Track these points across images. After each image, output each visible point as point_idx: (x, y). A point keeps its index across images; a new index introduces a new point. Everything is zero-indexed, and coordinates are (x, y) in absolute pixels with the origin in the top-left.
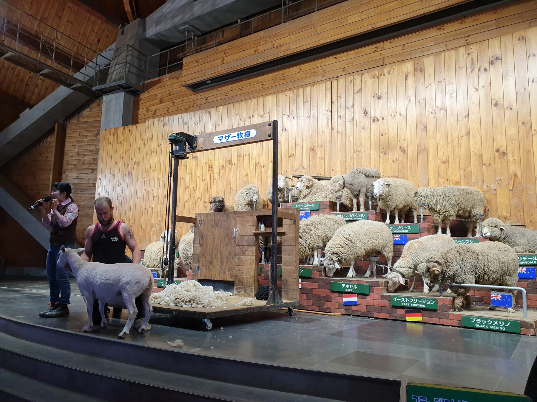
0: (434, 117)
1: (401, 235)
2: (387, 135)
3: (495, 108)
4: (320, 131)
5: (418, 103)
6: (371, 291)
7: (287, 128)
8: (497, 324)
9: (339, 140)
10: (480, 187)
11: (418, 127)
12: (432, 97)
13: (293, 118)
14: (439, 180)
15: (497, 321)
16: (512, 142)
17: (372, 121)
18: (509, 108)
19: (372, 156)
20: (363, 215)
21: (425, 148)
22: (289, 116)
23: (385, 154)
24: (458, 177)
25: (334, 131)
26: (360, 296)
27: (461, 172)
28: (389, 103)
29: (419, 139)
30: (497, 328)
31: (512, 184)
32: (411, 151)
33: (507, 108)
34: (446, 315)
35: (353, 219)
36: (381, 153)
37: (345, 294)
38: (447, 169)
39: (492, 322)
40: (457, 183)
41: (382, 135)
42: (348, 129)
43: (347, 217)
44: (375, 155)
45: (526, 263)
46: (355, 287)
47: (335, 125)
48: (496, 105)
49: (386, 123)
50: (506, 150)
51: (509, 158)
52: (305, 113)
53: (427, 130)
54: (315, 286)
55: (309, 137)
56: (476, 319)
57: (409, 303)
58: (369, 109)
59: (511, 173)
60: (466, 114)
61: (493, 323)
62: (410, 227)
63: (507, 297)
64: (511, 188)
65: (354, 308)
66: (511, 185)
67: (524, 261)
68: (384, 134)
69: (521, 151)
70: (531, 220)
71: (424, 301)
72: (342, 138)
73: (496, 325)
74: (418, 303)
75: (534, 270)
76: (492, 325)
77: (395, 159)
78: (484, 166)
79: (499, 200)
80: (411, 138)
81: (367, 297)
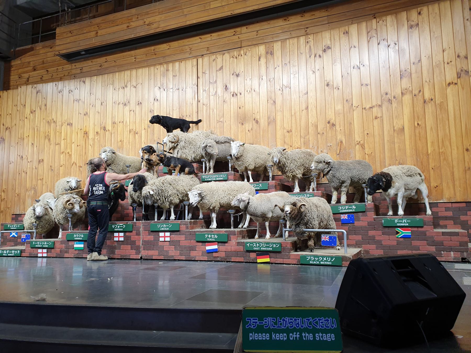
2: (244, 108)
3: (327, 88)
6: (230, 239)
7: (159, 99)
9: (204, 111)
13: (163, 90)
17: (231, 96)
18: (337, 88)
22: (160, 88)
23: (242, 124)
26: (220, 244)
27: (302, 140)
28: (245, 80)
29: (269, 112)
31: (339, 150)
32: (263, 122)
35: (216, 179)
36: (239, 124)
38: (291, 137)
39: (322, 258)
41: (240, 108)
42: (212, 102)
43: (211, 178)
45: (347, 211)
46: (216, 237)
47: (201, 98)
48: (328, 85)
49: (243, 98)
51: (337, 128)
52: (174, 86)
54: (182, 238)
55: (178, 108)
56: (310, 257)
58: (229, 85)
61: (323, 259)
65: (215, 255)
68: (241, 107)
69: (345, 123)
71: (271, 245)
72: (207, 110)
74: (266, 247)
76: (322, 261)
80: (263, 111)
81: (226, 244)
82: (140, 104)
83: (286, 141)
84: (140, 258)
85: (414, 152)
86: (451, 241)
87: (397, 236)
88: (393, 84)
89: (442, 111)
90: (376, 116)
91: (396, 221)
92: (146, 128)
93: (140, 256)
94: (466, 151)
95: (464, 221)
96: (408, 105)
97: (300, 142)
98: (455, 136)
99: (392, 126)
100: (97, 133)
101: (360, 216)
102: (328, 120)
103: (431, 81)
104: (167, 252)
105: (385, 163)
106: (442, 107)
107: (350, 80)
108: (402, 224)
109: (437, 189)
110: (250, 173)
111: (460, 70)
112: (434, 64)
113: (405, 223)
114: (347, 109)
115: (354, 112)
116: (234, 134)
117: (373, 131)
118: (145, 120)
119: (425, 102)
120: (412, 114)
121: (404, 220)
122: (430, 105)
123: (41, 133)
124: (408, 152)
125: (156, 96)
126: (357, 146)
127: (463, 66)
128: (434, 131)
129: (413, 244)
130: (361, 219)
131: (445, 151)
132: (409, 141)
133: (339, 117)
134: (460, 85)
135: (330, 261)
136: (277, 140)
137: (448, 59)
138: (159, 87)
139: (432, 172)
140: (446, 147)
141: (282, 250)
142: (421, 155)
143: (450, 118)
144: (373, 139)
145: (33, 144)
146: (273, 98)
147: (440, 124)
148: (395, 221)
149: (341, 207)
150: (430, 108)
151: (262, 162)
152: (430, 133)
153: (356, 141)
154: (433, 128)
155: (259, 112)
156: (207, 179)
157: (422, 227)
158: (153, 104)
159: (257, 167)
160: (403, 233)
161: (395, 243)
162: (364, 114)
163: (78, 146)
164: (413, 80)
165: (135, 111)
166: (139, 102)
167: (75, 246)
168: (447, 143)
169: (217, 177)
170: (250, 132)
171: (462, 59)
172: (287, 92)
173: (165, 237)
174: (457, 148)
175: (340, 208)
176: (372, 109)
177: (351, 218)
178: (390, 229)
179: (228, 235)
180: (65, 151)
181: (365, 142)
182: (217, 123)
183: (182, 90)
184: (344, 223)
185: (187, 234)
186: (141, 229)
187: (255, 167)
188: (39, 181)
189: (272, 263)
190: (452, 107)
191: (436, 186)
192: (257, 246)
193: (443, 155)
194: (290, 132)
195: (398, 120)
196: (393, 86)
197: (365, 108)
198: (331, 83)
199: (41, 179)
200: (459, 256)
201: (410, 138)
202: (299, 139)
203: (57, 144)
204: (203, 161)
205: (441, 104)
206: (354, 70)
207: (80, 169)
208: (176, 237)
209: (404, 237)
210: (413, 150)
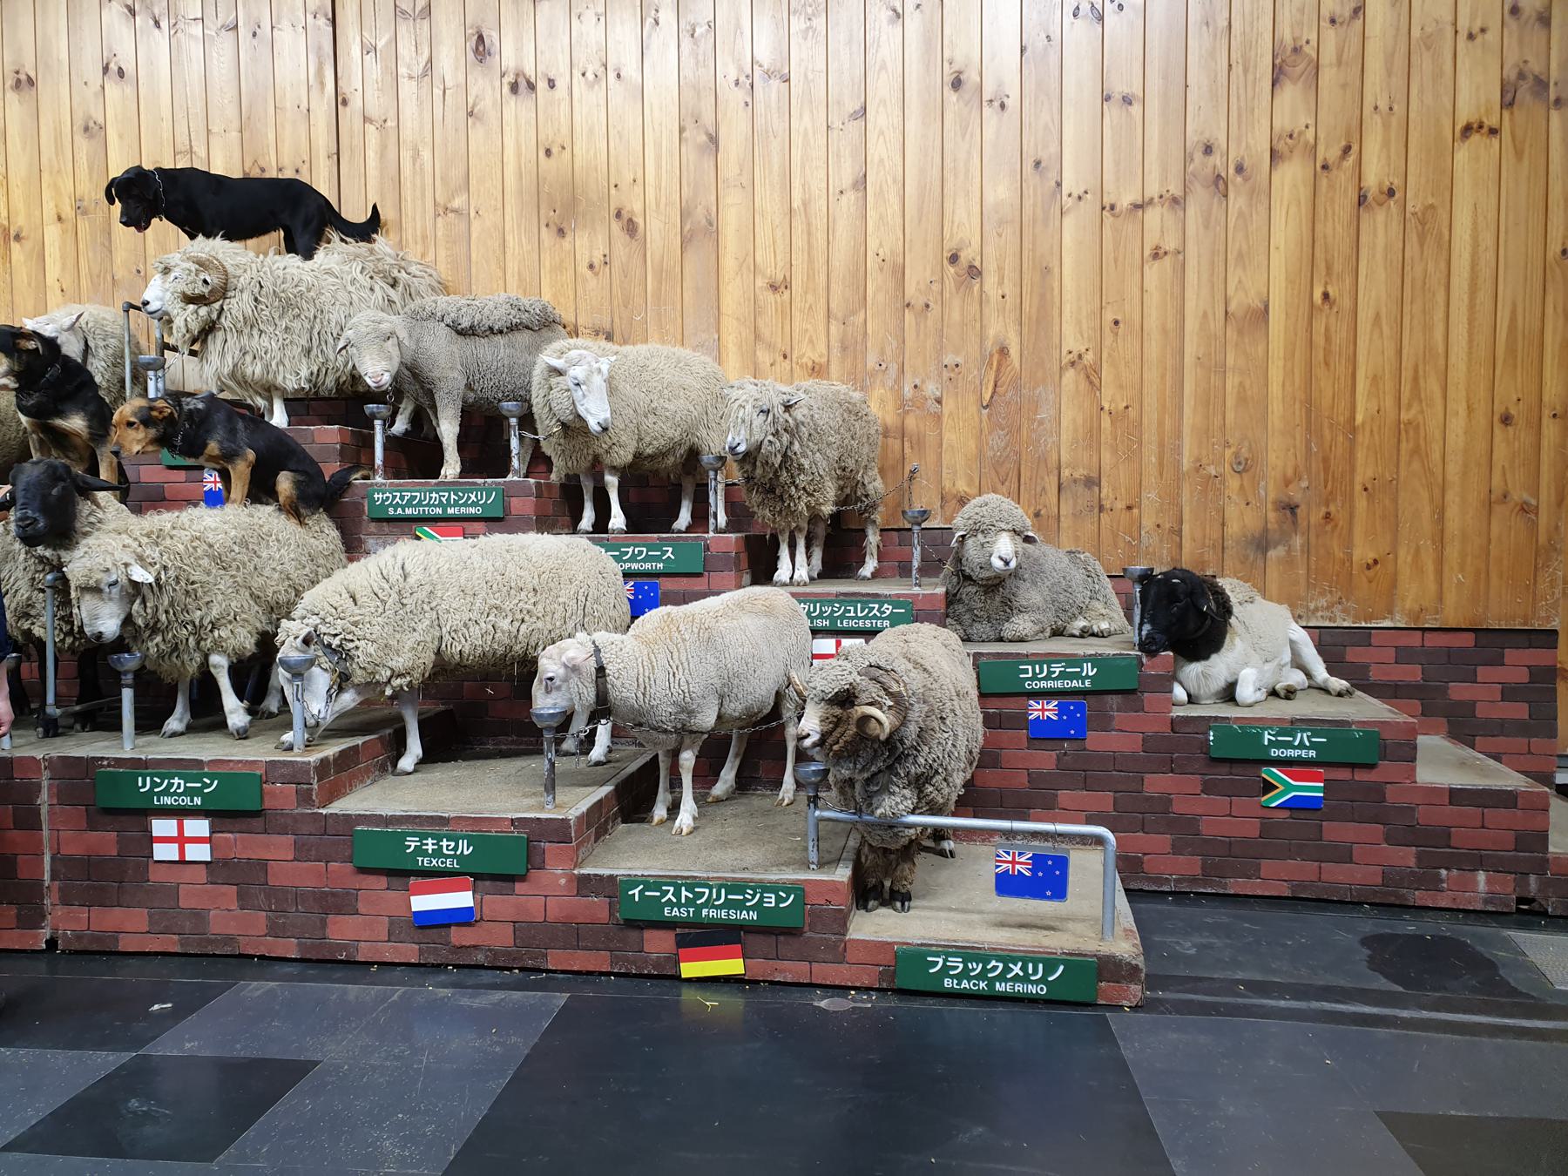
0: (747, 105)
1: (639, 580)
2: (567, 154)
3: (951, 97)
4: (288, 105)
5: (688, 35)
6: (537, 860)
7: (129, 68)
8: (1021, 974)
9: (371, 154)
10: (892, 389)
11: (684, 135)
12: (738, 20)
13: (152, 22)
14: (758, 352)
15: (1020, 964)
16: (1000, 230)
17: (506, 89)
18: (996, 104)
19: (509, 238)
20: (488, 498)
21: (711, 224)
22: (132, 12)
23: (561, 232)
24: (822, 348)
25: (348, 109)
26: (488, 883)
27: (833, 329)
28: (574, 19)
29: (689, 185)
30: (1019, 987)
31: (991, 384)
32: (660, 231)
33: (991, 101)
34: (835, 946)
35: (445, 511)
36: (544, 229)
37: (420, 880)
38: (787, 313)
39: (1001, 966)
40: (817, 371)
41: (548, 152)
42: (409, 109)
43: (420, 504)
44: (519, 234)
45: (1059, 684)
46: (465, 849)
47: (352, 83)
48: (957, 84)
49: (565, 106)
50: (979, 258)
51: (986, 288)
52: (210, 10)
53: (717, 151)
54: (275, 848)
55: (236, 124)
56: (945, 961)
57: (695, 906)
58: (495, 35)
59: (989, 344)
60: (857, 107)
61: (1007, 969)
62: (670, 549)
63: (1050, 863)
64: (987, 396)
65: (458, 936)
66: (987, 388)
67: (1054, 679)
68: (555, 150)
69: (1025, 266)
70: (1040, 510)
71: (753, 896)
72: (383, 148)
73: (1016, 978)
74: (728, 904)
75: (1080, 708)
76: (1002, 978)
77: (597, 259)
78: (907, 311)
79: (949, 437)
80: (658, 176)
81: (518, 886)
83: (765, 331)
84: (44, 946)
85: (1297, 413)
86: (1483, 827)
87: (1263, 799)
88: (1239, 108)
89: (1425, 247)
90: (1158, 248)
91: (1267, 736)
92: (68, 212)
93: (46, 933)
94: (1503, 426)
95: (1461, 704)
96: (1293, 209)
97: (823, 338)
98: (1465, 358)
99: (1219, 297)
101: (1112, 710)
102: (949, 245)
103: (1395, 107)
104: (199, 915)
105: (1180, 454)
106: (1427, 228)
107: (1057, 73)
108: (1291, 753)
109: (1376, 575)
110: (612, 481)
111: (1517, 70)
112: (1416, 32)
113: (1306, 747)
114: (1035, 205)
115: (1068, 221)
116: (519, 274)
117: (1138, 309)
118: (59, 171)
119: (1362, 200)
120: (1307, 250)
121: (1299, 735)
122: (1380, 216)
124: (1276, 408)
125: (110, 50)
126: (1070, 374)
127: (1529, 58)
128: (1386, 329)
129: (1325, 836)
130: (1115, 724)
131: (1420, 418)
132: (1285, 366)
133: (1000, 235)
134: (1509, 139)
135: (1043, 980)
136: (725, 321)
137: (1473, 17)
138: (128, 7)
139: (1361, 503)
140: (1424, 404)
141: (808, 920)
142: (1327, 433)
143: (1455, 281)
144: (1138, 347)
146: (708, 118)
147: (1412, 303)
148: (1261, 736)
149: (1030, 667)
150: (1380, 227)
151: (670, 433)
152: (1371, 340)
153: (1064, 352)
154: (1383, 315)
155: (640, 181)
156: (399, 511)
157: (1371, 766)
158: (96, 94)
159: (649, 456)
160: (1289, 788)
161: (1251, 829)
162: (1107, 232)
164: (1323, 93)
166: (23, 77)
168: (1432, 386)
169: (448, 499)
171: (1526, 22)
172: (774, 96)
173: (181, 840)
174: (1470, 409)
175: (1026, 671)
176: (1141, 212)
177: (1071, 714)
178: (1237, 769)
179: (529, 841)
181: (1105, 356)
182: (437, 215)
183: (254, 35)
184: (1042, 734)
185: (305, 829)
186: (44, 798)
187: (638, 456)
189: (754, 982)
190: (1469, 232)
191: (1370, 561)
192: (679, 898)
193: (1411, 433)
194: (783, 288)
195: (1244, 269)
196: (1239, 116)
197: (1112, 207)
198: (971, 77)
200: (1507, 887)
201: (1289, 355)
202: (822, 328)
204: (374, 416)
205: (1424, 214)
206: (1078, 22)
208: (245, 845)
209: (1294, 806)
210: (1297, 406)
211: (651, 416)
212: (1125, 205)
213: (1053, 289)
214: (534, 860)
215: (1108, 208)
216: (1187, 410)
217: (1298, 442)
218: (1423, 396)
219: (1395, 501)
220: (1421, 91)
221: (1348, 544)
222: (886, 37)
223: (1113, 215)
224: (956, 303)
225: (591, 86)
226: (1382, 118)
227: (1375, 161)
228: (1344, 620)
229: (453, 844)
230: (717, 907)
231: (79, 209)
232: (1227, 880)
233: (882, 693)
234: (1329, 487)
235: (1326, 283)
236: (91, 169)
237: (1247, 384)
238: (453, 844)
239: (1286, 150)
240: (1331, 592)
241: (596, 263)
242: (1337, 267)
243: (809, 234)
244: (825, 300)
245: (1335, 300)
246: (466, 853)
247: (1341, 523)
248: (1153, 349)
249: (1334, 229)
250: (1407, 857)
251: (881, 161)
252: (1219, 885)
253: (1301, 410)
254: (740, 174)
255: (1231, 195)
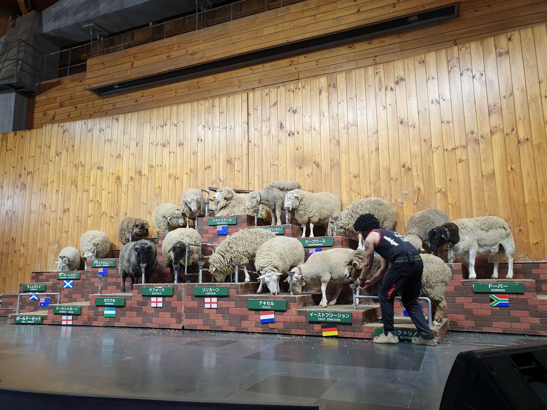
0: (347, 133)
1: (317, 248)
3: (400, 126)
4: (237, 144)
6: (289, 307)
7: (203, 139)
9: (256, 153)
12: (344, 113)
15: (406, 331)
17: (287, 135)
18: (413, 126)
19: (288, 170)
21: (338, 163)
22: (204, 127)
23: (301, 168)
26: (277, 312)
27: (372, 186)
31: (416, 198)
32: (325, 166)
36: (296, 167)
38: (359, 183)
39: (401, 332)
41: (297, 149)
42: (265, 142)
46: (272, 304)
47: (252, 138)
48: (402, 123)
49: (301, 138)
54: (230, 304)
55: (226, 149)
57: (326, 318)
58: (285, 123)
61: (403, 333)
62: (324, 240)
64: (416, 202)
65: (271, 326)
68: (299, 148)
69: (423, 167)
72: (259, 151)
74: (333, 317)
80: (325, 152)
82: (181, 144)
83: (353, 188)
87: (491, 304)
88: (480, 122)
89: (540, 154)
91: (490, 286)
92: (189, 172)
93: (182, 325)
96: (499, 146)
99: (480, 171)
100: (131, 178)
103: (526, 117)
104: (214, 321)
109: (538, 246)
110: (312, 226)
112: (529, 98)
114: (425, 151)
117: (456, 176)
119: (519, 142)
120: (504, 157)
122: (525, 146)
123: (68, 179)
126: (439, 194)
128: (531, 177)
138: (204, 126)
139: (530, 226)
142: (517, 206)
145: (57, 191)
146: (337, 137)
150: (525, 150)
151: (327, 213)
153: (436, 189)
157: (522, 294)
158: (196, 145)
159: (322, 219)
160: (498, 300)
161: (489, 313)
162: (446, 157)
163: (109, 193)
165: (175, 153)
166: (181, 143)
167: (106, 312)
170: (309, 177)
173: (211, 303)
176: (455, 151)
178: (483, 295)
180: (94, 199)
181: (448, 189)
185: (238, 300)
187: (320, 220)
188: (64, 234)
191: (536, 243)
192: (322, 315)
193: (544, 205)
195: (486, 163)
196: (480, 124)
198: (405, 120)
199: (65, 232)
201: (503, 185)
202: (368, 186)
203: (85, 191)
205: (539, 145)
207: (111, 220)
208: (224, 303)
209: (501, 306)
210: (507, 199)
211: (323, 209)
212: (450, 149)
213: (432, 172)
214: (288, 307)
215: (445, 150)
216: (474, 203)
217: (508, 210)
218: (546, 194)
219: (541, 225)
220: (533, 113)
221: (528, 238)
222: (382, 114)
223: (447, 152)
224: (405, 178)
225: (308, 132)
226: (522, 120)
227: (522, 132)
228: (530, 261)
229: (270, 303)
230: (331, 318)
231: (191, 171)
232: (483, 328)
233: (359, 259)
234: (519, 222)
235: (511, 165)
236: (194, 162)
237: (491, 194)
238: (270, 303)
239: (495, 131)
240: (524, 252)
241: (309, 175)
242: (514, 160)
243: (364, 163)
244: (369, 179)
245: (515, 170)
246: (273, 305)
247: (525, 232)
248: (462, 186)
249: (512, 151)
250: (537, 321)
251: (382, 143)
252: (481, 329)
253: (508, 200)
254: (346, 150)
255: (480, 144)
